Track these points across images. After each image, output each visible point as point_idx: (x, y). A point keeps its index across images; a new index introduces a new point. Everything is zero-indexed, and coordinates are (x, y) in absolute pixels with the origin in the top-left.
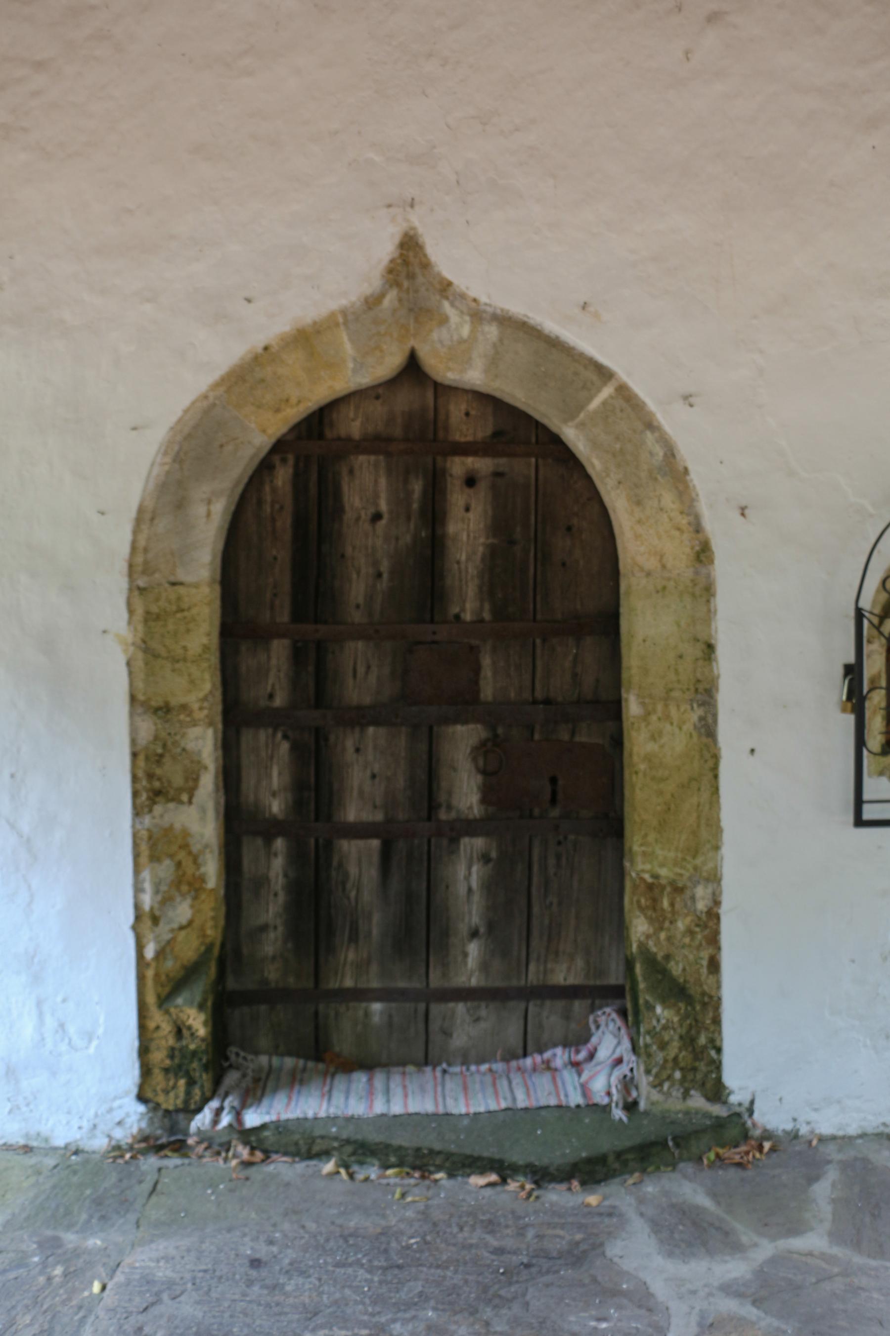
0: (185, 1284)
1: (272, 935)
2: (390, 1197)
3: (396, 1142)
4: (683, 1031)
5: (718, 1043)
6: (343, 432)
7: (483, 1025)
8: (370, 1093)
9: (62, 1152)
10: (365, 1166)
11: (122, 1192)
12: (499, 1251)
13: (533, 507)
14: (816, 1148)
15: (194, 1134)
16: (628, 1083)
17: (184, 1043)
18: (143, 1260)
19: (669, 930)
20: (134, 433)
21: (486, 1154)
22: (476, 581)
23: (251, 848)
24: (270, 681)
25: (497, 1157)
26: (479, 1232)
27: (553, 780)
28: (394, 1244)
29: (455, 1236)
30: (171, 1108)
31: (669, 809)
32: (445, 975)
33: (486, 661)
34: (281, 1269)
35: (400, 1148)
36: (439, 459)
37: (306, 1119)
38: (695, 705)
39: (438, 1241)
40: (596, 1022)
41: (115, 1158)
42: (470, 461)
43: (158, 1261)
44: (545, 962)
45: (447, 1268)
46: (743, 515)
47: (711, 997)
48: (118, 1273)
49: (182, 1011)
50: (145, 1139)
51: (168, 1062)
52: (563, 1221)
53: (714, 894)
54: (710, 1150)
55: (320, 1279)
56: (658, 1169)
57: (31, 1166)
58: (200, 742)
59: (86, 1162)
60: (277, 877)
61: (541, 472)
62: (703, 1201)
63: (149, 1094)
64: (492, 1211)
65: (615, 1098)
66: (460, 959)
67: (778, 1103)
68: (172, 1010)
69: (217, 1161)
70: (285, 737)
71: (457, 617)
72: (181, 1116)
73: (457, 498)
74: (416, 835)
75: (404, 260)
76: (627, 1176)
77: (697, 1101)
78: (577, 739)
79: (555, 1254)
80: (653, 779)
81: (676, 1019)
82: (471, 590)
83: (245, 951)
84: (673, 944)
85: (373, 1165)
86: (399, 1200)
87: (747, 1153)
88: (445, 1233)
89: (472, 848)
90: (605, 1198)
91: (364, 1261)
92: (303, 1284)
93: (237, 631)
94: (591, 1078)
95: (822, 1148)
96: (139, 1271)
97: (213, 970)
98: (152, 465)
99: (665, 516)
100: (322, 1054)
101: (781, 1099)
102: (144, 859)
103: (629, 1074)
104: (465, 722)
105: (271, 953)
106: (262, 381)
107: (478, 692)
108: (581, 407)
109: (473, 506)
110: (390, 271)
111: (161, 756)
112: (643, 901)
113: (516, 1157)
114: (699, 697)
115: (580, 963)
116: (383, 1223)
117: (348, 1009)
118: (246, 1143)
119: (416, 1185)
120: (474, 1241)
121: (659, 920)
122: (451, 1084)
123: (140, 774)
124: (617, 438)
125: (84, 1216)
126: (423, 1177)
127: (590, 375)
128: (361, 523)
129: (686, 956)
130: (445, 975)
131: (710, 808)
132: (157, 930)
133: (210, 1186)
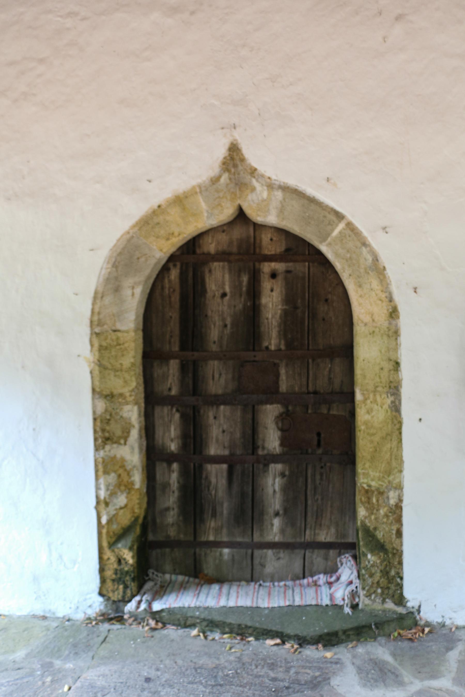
0: (110, 689)
1: (172, 513)
2: (223, 649)
3: (229, 621)
4: (382, 568)
5: (401, 575)
6: (205, 250)
7: (281, 561)
8: (220, 594)
9: (61, 620)
10: (213, 633)
11: (88, 641)
12: (274, 680)
13: (307, 289)
14: (454, 632)
15: (127, 613)
16: (354, 594)
17: (122, 567)
18: (92, 676)
19: (376, 514)
20: (91, 252)
21: (274, 629)
22: (277, 329)
23: (160, 468)
25: (280, 630)
26: (266, 669)
27: (319, 434)
28: (220, 674)
29: (252, 670)
30: (116, 599)
31: (376, 450)
33: (283, 371)
34: (160, 684)
35: (230, 624)
37: (184, 607)
38: (389, 395)
39: (244, 673)
40: (340, 561)
41: (87, 624)
42: (274, 265)
43: (99, 676)
44: (315, 529)
45: (245, 687)
46: (415, 292)
47: (397, 550)
48: (78, 682)
50: (103, 615)
51: (114, 576)
52: (311, 665)
53: (399, 496)
54: (395, 631)
55: (179, 690)
56: (366, 640)
57: (45, 626)
58: (130, 413)
59: (73, 625)
62: (388, 658)
63: (105, 592)
64: (275, 658)
65: (346, 602)
66: (269, 527)
67: (434, 607)
68: (116, 550)
69: (139, 627)
71: (267, 348)
72: (121, 604)
73: (266, 284)
74: (246, 462)
75: (231, 158)
76: (349, 643)
77: (390, 605)
78: (331, 412)
79: (303, 682)
80: (368, 434)
81: (378, 561)
82: (274, 333)
83: (158, 520)
84: (378, 522)
85: (217, 632)
86: (228, 650)
88: (248, 669)
89: (275, 470)
90: (335, 654)
91: (203, 681)
92: (170, 692)
93: (151, 355)
94: (336, 591)
95: (457, 633)
96: (88, 681)
97: (138, 530)
98: (102, 269)
99: (374, 293)
100: (197, 574)
101: (435, 605)
102: (100, 473)
103: (355, 589)
104: (272, 403)
105: (171, 522)
106: (158, 223)
107: (278, 387)
108: (329, 235)
109: (275, 288)
110: (224, 163)
111: (109, 420)
112: (363, 499)
113: (290, 631)
114: (391, 390)
115: (333, 530)
116: (217, 662)
117: (211, 551)
118: (153, 618)
119: (238, 643)
120: (262, 674)
121: (371, 509)
122: (263, 592)
123: (98, 429)
124: (348, 251)
125: (67, 652)
126: (242, 639)
127: (332, 217)
128: (215, 298)
129: (384, 529)
130: (261, 535)
131: (397, 450)
132: (108, 509)
133: (133, 640)
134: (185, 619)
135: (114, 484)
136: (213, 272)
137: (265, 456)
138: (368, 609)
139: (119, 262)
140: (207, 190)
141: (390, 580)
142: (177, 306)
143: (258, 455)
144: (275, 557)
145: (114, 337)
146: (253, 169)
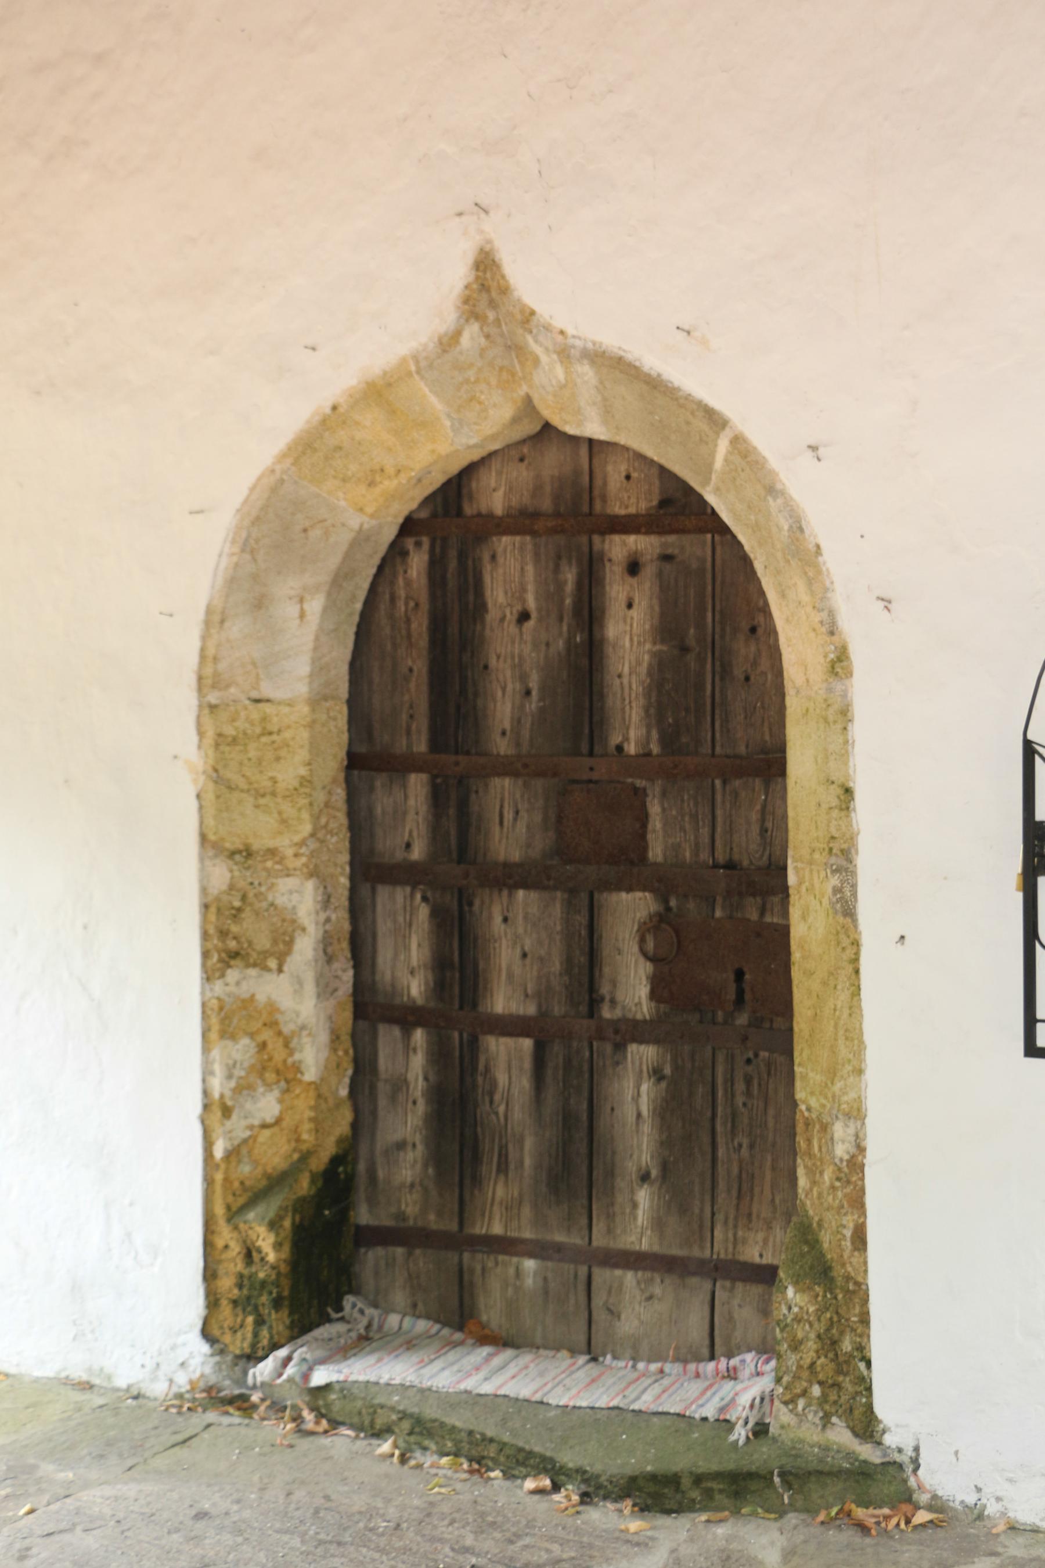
1: (410, 1155)
17: (254, 1270)
22: (642, 701)
27: (739, 975)
32: (610, 1231)
33: (654, 808)
36: (596, 539)
42: (635, 542)
44: (735, 1226)
47: (858, 1284)
49: (251, 1228)
51: (236, 1291)
53: (857, 1136)
58: (295, 897)
60: (417, 1080)
61: (718, 549)
63: (216, 1332)
68: (242, 1226)
70: (425, 899)
71: (619, 748)
73: (617, 589)
74: (574, 1038)
75: (483, 285)
77: (840, 1435)
81: (811, 1309)
82: (635, 714)
83: (381, 1174)
87: (887, 1518)
89: (641, 1059)
93: (366, 762)
98: (220, 556)
104: (630, 889)
105: (409, 1180)
106: (339, 448)
107: (645, 849)
108: (709, 467)
110: (466, 301)
111: (239, 910)
114: (833, 860)
117: (497, 1263)
123: (212, 931)
127: (701, 424)
130: (610, 1231)
132: (228, 1124)
134: (371, 1410)
135: (246, 1065)
136: (500, 560)
137: (616, 1025)
138: (786, 1437)
139: (257, 541)
140: (431, 366)
142: (423, 642)
143: (600, 1017)
144: (642, 1290)
145: (255, 716)
146: (528, 311)
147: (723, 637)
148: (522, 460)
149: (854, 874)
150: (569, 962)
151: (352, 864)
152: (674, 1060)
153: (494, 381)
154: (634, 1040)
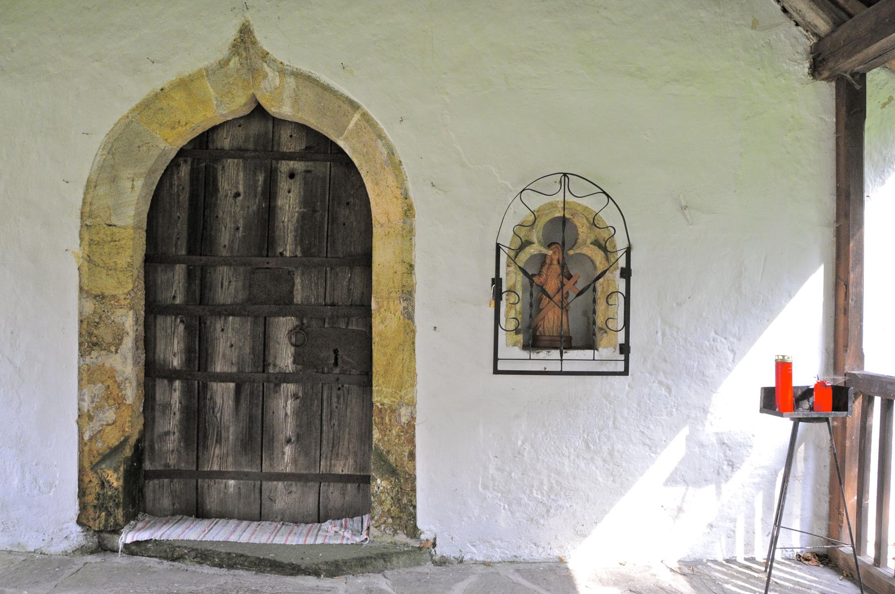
5: (414, 503)
7: (294, 496)
23: (161, 386)
24: (174, 288)
33: (298, 281)
36: (274, 162)
47: (410, 475)
63: (85, 521)
70: (182, 321)
71: (281, 254)
73: (284, 184)
74: (256, 382)
77: (401, 538)
82: (290, 238)
83: (156, 447)
93: (154, 258)
102: (84, 382)
104: (285, 315)
107: (293, 298)
108: (345, 128)
110: (234, 46)
127: (346, 107)
137: (276, 376)
141: (403, 509)
143: (269, 373)
147: (333, 206)
148: (240, 126)
149: (413, 301)
150: (253, 349)
151: (145, 305)
152: (304, 390)
153: (240, 85)
154: (285, 382)
